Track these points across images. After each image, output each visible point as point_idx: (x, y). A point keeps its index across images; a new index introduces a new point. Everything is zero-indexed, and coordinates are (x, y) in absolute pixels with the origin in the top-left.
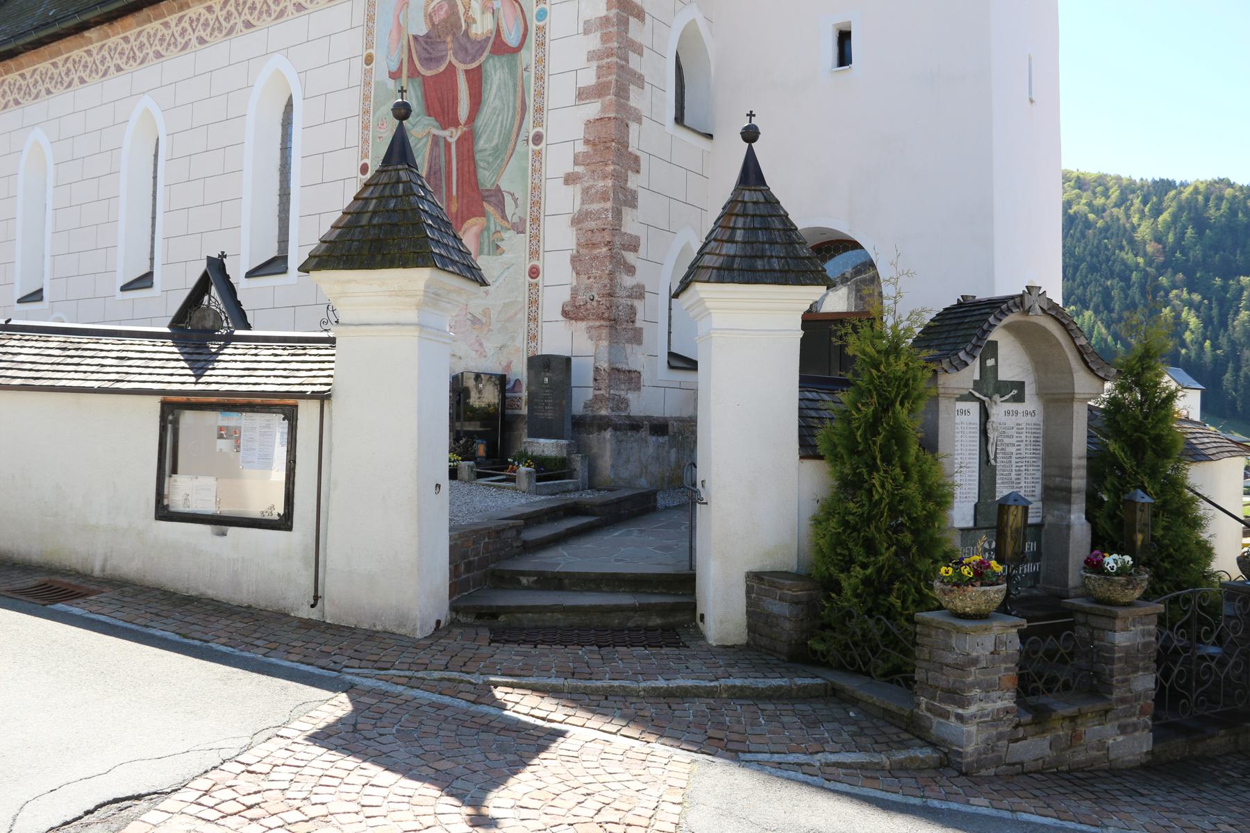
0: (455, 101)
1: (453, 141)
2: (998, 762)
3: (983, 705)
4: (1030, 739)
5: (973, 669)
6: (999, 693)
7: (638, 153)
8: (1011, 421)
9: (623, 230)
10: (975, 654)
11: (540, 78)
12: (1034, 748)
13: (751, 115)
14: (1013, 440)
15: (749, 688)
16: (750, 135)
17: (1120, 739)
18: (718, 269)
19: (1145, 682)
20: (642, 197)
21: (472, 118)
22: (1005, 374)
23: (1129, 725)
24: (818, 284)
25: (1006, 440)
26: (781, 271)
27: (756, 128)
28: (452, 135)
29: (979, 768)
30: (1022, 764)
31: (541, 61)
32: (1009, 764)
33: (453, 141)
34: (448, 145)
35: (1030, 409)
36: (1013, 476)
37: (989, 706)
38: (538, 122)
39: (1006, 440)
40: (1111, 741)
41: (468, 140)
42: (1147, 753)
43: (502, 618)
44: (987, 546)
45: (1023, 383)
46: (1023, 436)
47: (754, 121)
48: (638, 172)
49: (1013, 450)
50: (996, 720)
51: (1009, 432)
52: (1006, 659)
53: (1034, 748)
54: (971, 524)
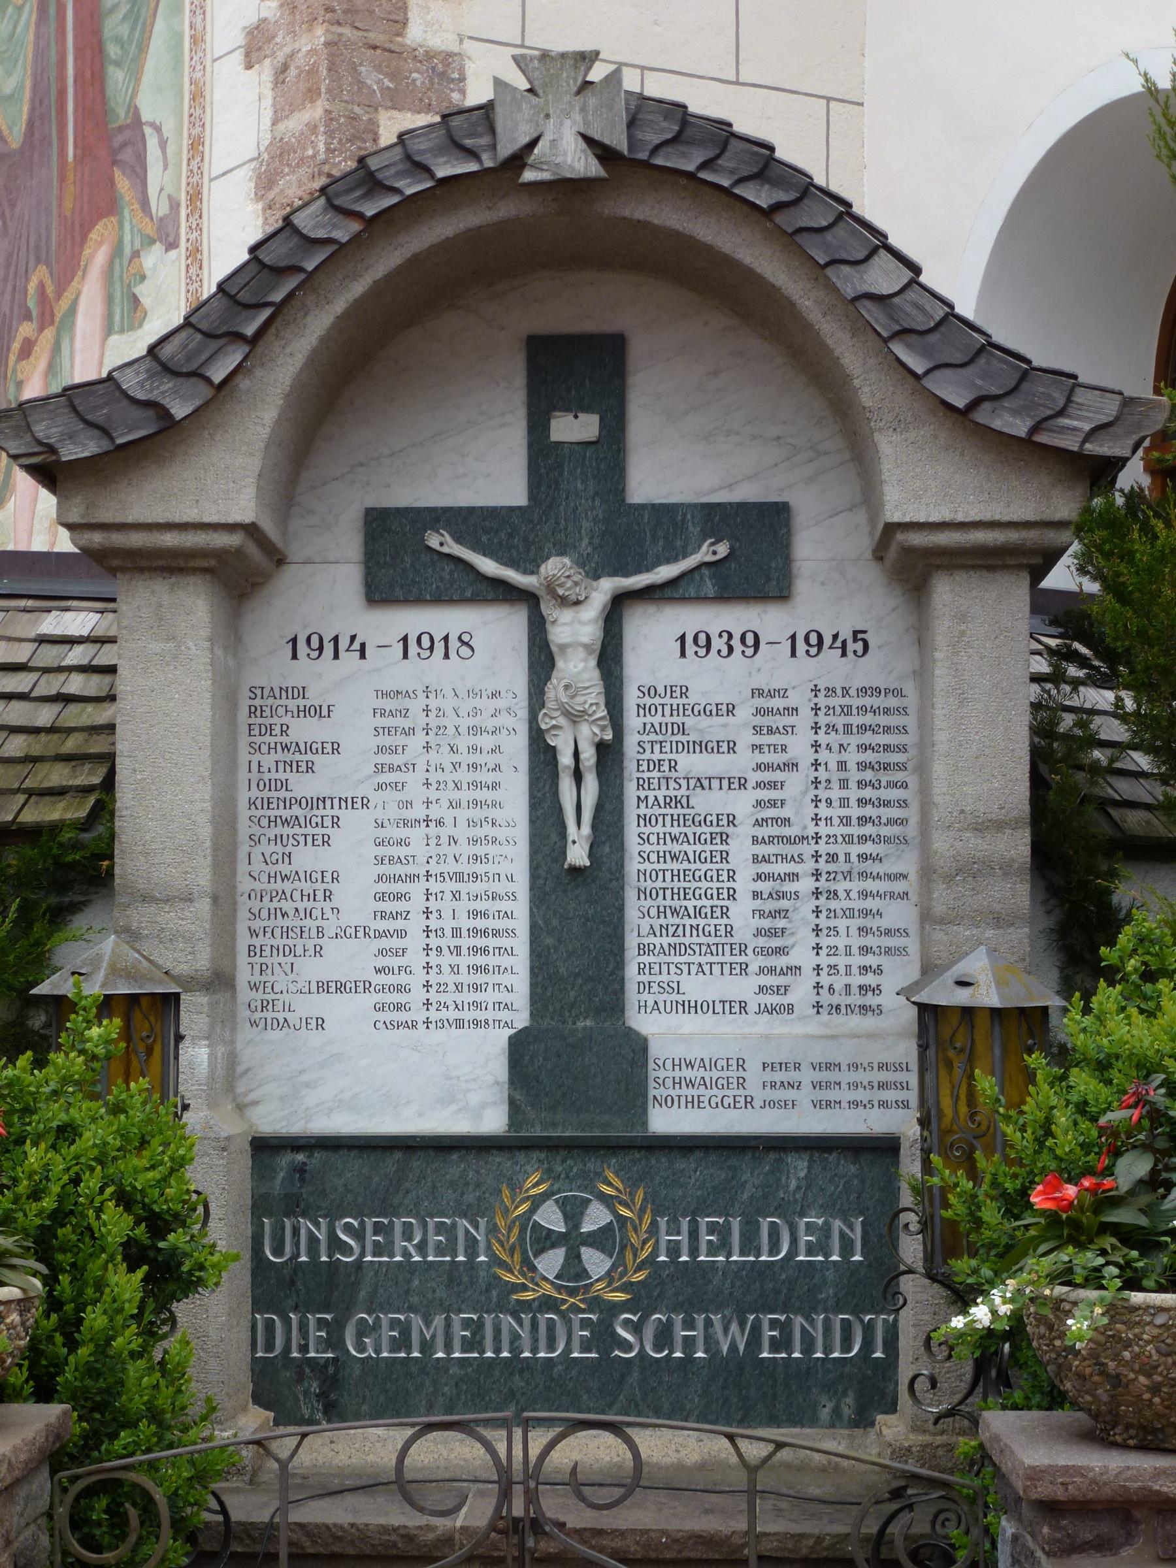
8: (709, 679)
14: (742, 762)
36: (742, 916)
39: (691, 763)
46: (799, 747)
49: (742, 804)
54: (493, 1121)
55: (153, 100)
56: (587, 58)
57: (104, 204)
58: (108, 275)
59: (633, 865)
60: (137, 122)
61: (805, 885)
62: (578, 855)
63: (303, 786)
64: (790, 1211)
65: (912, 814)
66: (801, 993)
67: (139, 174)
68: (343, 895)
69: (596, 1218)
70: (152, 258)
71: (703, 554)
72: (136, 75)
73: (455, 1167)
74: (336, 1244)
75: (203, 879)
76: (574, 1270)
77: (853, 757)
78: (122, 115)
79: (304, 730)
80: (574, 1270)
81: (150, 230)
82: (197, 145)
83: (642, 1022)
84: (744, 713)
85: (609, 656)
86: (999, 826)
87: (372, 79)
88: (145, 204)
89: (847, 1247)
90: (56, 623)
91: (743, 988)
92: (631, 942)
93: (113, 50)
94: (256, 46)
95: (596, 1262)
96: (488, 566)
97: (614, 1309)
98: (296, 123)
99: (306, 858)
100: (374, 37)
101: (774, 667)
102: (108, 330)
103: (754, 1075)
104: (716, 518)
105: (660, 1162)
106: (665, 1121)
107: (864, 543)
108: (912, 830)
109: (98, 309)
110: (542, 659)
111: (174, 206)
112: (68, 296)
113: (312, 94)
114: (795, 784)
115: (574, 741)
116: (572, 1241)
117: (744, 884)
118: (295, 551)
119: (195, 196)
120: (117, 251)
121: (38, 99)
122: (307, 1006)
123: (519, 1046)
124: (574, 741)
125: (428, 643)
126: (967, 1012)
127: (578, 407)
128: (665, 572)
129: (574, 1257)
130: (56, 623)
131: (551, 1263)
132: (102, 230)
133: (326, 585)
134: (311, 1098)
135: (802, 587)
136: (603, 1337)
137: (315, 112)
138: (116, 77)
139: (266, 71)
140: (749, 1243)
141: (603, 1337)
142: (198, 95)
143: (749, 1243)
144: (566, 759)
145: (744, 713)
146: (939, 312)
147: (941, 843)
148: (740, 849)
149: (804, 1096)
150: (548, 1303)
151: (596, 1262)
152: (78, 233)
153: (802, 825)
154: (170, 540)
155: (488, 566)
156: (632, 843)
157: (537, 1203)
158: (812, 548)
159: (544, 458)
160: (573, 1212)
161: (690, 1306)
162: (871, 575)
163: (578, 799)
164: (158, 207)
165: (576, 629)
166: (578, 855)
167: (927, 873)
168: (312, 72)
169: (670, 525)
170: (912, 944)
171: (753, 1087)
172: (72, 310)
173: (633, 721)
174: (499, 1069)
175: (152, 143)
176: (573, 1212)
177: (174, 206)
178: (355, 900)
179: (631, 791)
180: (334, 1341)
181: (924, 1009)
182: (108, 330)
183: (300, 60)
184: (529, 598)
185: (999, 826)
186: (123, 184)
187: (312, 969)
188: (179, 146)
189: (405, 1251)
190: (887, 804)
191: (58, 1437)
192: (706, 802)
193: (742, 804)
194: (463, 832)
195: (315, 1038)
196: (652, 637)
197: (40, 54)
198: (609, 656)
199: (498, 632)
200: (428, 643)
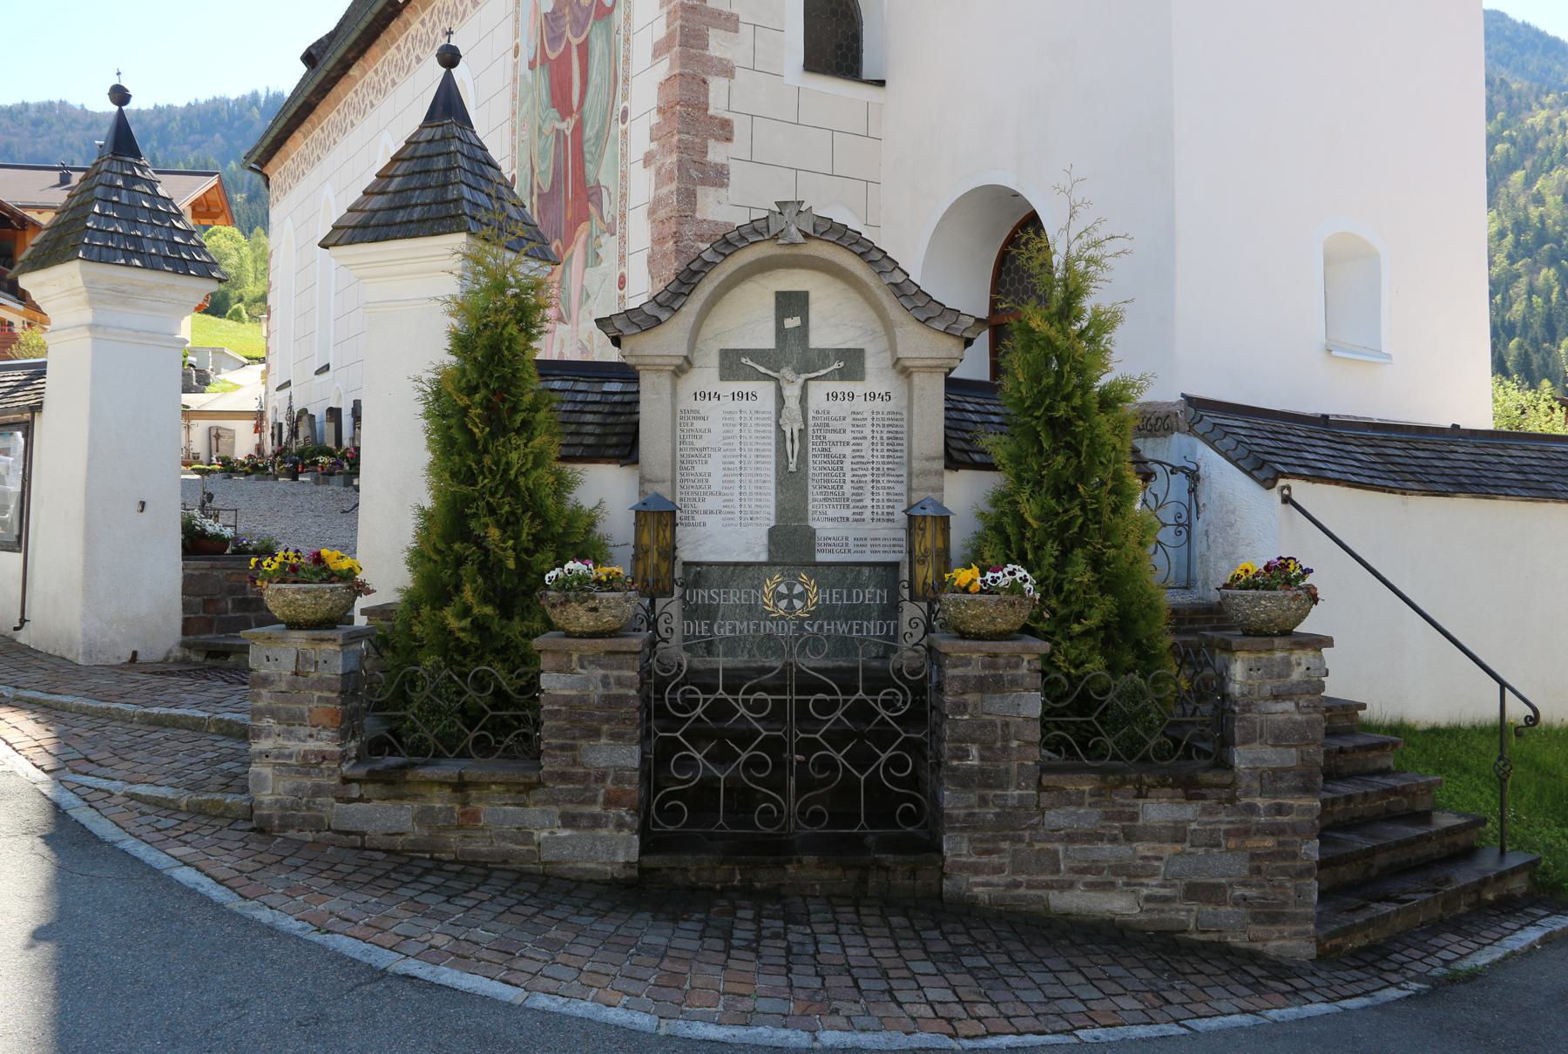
0: (570, 88)
1: (568, 133)
2: (318, 824)
3: (281, 741)
4: (375, 803)
5: (264, 692)
6: (308, 730)
7: (727, 116)
8: (837, 408)
9: (698, 215)
10: (263, 671)
11: (627, 40)
12: (386, 817)
13: (450, 33)
14: (848, 437)
15: (236, 723)
16: (450, 58)
17: (566, 833)
18: (354, 227)
19: (619, 756)
20: (736, 172)
21: (581, 103)
22: (821, 337)
23: (581, 815)
24: (450, 231)
25: (831, 437)
26: (419, 221)
27: (455, 49)
28: (567, 126)
29: (285, 826)
30: (362, 834)
31: (628, 18)
32: (337, 832)
33: (568, 133)
34: (566, 137)
35: (881, 389)
36: (847, 488)
37: (293, 746)
38: (625, 98)
39: (831, 437)
40: (545, 834)
41: (579, 128)
42: (628, 864)
43: (232, 659)
44: (783, 589)
45: (862, 351)
46: (867, 431)
47: (453, 38)
48: (728, 139)
49: (848, 450)
50: (309, 764)
51: (834, 424)
52: (320, 684)
53: (386, 817)
54: (763, 558)
55: (603, 174)
56: (800, 203)
57: (584, 216)
58: (586, 244)
59: (811, 471)
60: (599, 186)
61: (869, 478)
62: (792, 467)
63: (699, 444)
64: (863, 587)
65: (905, 454)
66: (867, 514)
67: (600, 206)
68: (712, 481)
69: (798, 589)
70: (605, 239)
71: (836, 366)
72: (598, 167)
73: (750, 572)
74: (711, 598)
75: (668, 474)
76: (791, 607)
77: (885, 435)
78: (592, 183)
79: (698, 424)
80: (791, 607)
81: (604, 227)
82: (624, 196)
83: (814, 524)
84: (849, 420)
85: (803, 399)
86: (934, 458)
87: (694, 173)
88: (602, 218)
89: (882, 598)
90: (608, 387)
91: (848, 513)
92: (810, 497)
93: (588, 156)
94: (648, 160)
95: (798, 604)
96: (762, 370)
97: (804, 619)
98: (665, 190)
99: (699, 468)
100: (696, 158)
101: (860, 405)
102: (586, 266)
103: (851, 542)
104: (841, 354)
105: (820, 569)
106: (820, 557)
107: (889, 362)
108: (905, 459)
109: (582, 258)
110: (781, 400)
111: (614, 219)
112: (569, 252)
113: (671, 179)
114: (866, 444)
115: (792, 426)
116: (790, 597)
117: (848, 478)
118: (696, 364)
119: (623, 216)
120: (590, 235)
121: (556, 173)
122: (699, 518)
123: (772, 532)
124: (792, 426)
125: (741, 395)
126: (924, 517)
127: (792, 316)
128: (823, 372)
129: (791, 602)
130: (608, 387)
131: (783, 604)
132: (584, 226)
133: (706, 375)
134: (701, 550)
135: (868, 377)
136: (800, 628)
137: (673, 186)
138: (589, 167)
139: (652, 170)
140: (849, 597)
141: (800, 628)
142: (624, 177)
143: (849, 597)
144: (788, 435)
145: (849, 420)
146: (915, 289)
147: (916, 465)
148: (847, 466)
149: (868, 549)
150: (782, 618)
151: (798, 604)
152: (573, 227)
153: (868, 458)
154: (658, 361)
155: (762, 370)
156: (811, 464)
157: (778, 584)
158: (870, 364)
159: (780, 331)
160: (790, 587)
161: (829, 619)
162: (892, 374)
163: (793, 448)
164: (608, 219)
165: (792, 393)
166: (792, 467)
167: (910, 475)
168: (671, 171)
169: (824, 355)
170: (905, 498)
171: (851, 547)
172: (571, 257)
173: (811, 422)
174: (765, 540)
175: (605, 194)
176: (790, 587)
177: (614, 219)
178: (716, 483)
179: (810, 446)
180: (710, 629)
181: (910, 517)
182: (586, 266)
183: (667, 166)
184: (776, 379)
185: (934, 458)
186: (592, 209)
187: (701, 506)
188: (616, 196)
189: (732, 600)
190: (620, 414)
191: (1125, 387)
192: (835, 450)
193: (848, 450)
194: (754, 459)
195: (702, 529)
196: (818, 392)
197: (556, 156)
198: (803, 399)
199: (765, 390)
200: (741, 395)
